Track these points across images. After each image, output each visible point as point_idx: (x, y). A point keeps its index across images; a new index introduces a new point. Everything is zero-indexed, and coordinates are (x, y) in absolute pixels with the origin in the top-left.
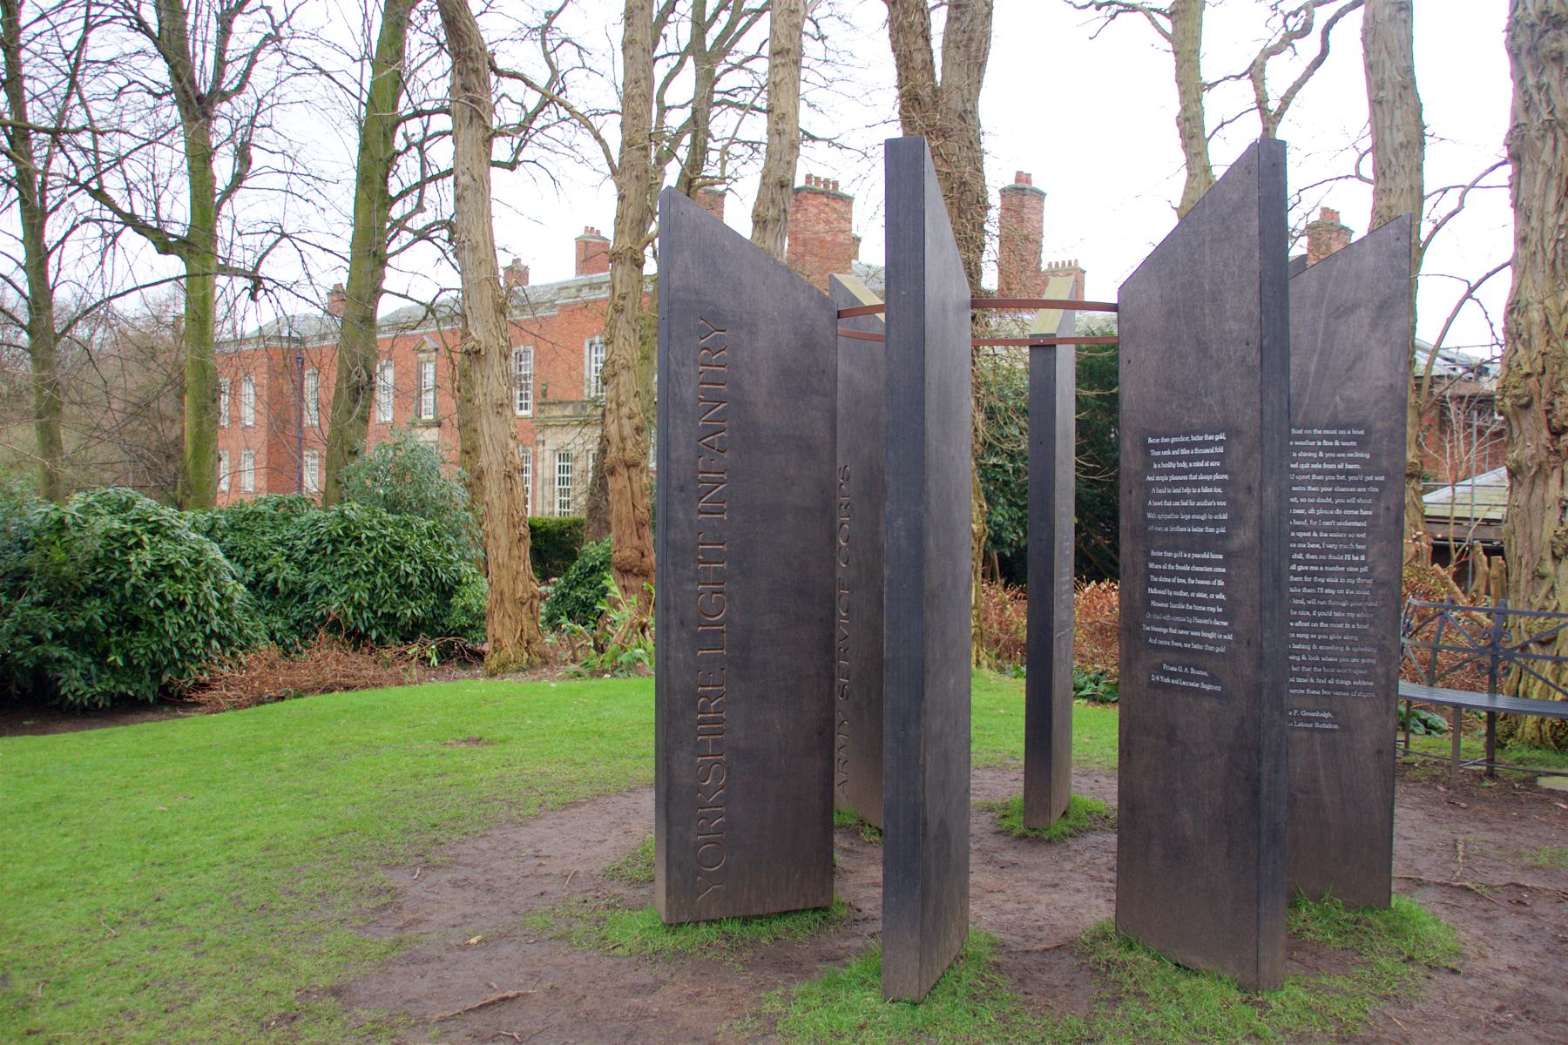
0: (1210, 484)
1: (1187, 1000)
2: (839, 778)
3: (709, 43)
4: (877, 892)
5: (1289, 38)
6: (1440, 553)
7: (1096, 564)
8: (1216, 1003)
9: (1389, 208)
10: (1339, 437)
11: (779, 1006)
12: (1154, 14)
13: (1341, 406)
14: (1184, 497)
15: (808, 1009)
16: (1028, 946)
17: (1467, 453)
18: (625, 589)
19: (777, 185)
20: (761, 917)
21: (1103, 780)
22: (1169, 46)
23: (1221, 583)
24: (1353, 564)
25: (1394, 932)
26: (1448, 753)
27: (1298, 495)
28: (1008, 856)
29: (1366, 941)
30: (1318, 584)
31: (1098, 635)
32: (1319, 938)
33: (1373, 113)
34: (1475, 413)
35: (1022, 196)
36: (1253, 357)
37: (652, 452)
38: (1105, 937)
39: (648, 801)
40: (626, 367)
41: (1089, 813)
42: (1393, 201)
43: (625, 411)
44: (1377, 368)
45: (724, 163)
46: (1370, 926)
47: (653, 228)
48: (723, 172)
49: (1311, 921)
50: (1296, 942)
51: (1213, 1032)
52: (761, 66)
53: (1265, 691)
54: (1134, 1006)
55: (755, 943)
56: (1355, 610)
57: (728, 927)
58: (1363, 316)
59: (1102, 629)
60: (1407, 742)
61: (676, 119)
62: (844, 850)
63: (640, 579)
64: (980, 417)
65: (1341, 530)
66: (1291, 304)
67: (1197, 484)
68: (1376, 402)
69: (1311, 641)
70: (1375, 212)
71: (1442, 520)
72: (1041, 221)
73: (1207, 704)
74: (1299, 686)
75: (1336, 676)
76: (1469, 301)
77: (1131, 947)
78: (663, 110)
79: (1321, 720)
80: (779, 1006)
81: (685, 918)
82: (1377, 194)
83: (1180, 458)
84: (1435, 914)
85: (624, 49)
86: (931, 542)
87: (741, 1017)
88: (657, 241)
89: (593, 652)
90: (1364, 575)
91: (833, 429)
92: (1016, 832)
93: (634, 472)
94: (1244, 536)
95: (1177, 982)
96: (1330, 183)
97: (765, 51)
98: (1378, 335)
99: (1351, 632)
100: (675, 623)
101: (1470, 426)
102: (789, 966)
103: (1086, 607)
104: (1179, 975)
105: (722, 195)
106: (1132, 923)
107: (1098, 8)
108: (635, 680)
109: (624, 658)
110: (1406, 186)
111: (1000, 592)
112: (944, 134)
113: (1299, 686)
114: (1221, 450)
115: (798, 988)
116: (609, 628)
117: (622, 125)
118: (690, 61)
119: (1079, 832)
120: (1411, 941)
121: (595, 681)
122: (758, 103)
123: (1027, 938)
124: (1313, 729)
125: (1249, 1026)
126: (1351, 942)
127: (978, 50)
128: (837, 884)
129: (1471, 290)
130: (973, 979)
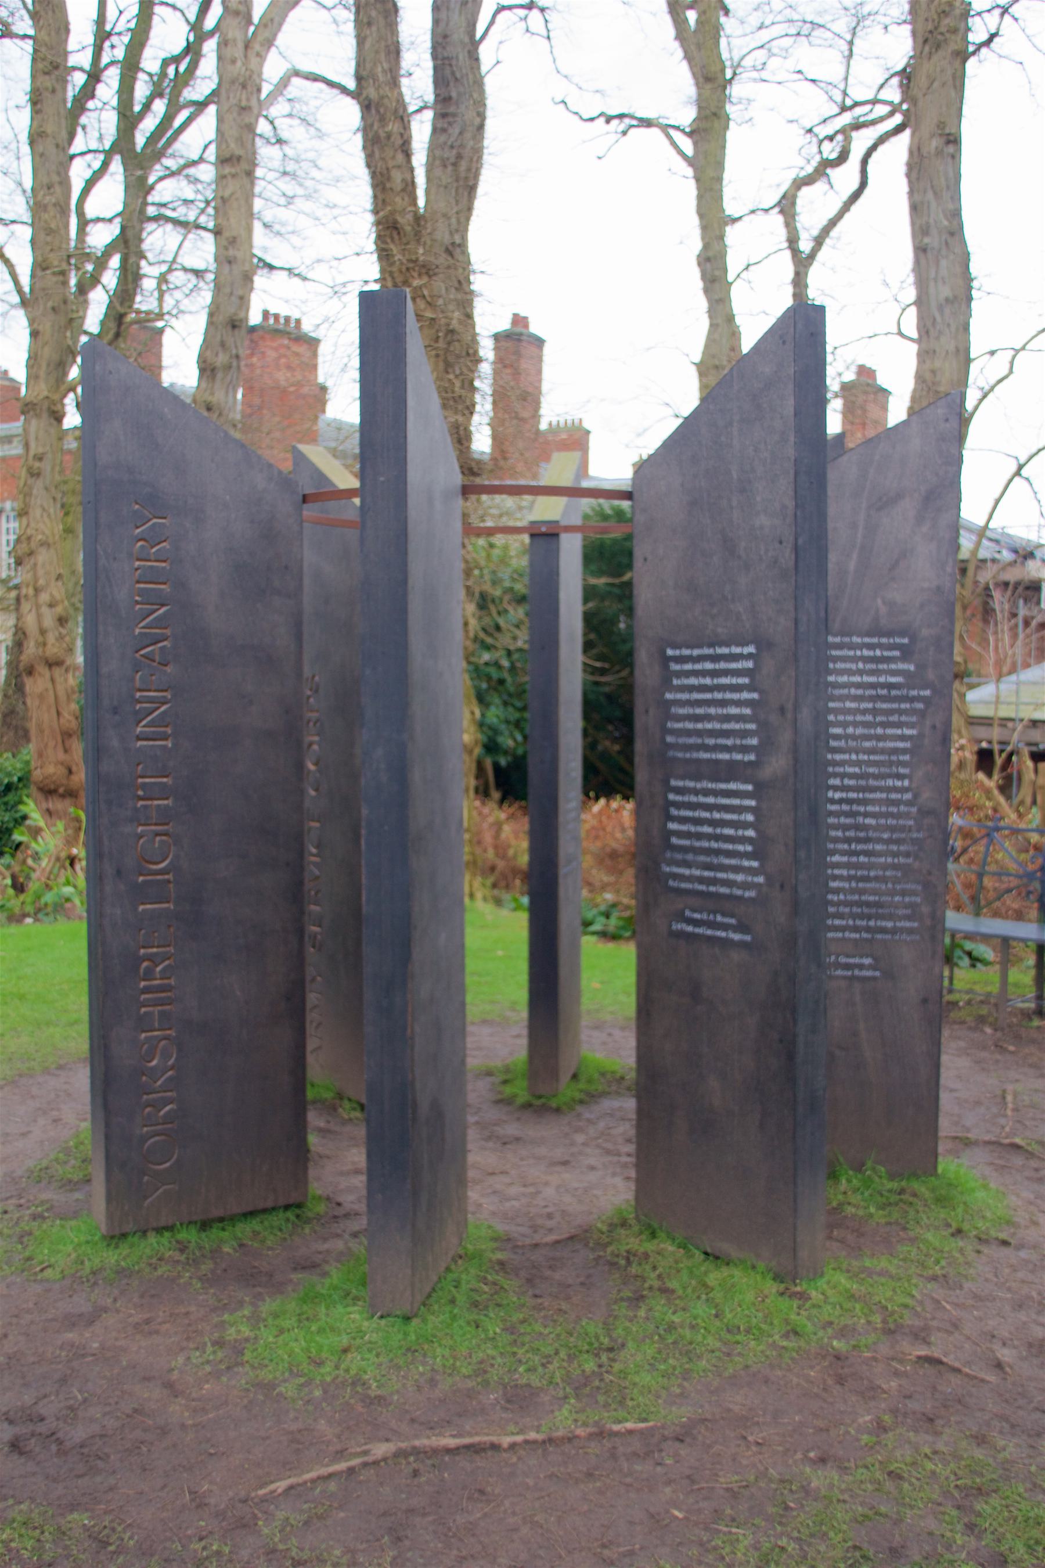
0: (738, 703)
1: (718, 1295)
2: (311, 1044)
3: (140, 140)
4: (360, 1181)
5: (825, 165)
6: (985, 759)
7: (607, 777)
8: (750, 1296)
9: (933, 372)
10: (880, 646)
11: (246, 1331)
12: (672, 132)
13: (883, 610)
14: (707, 718)
15: (281, 1331)
16: (537, 1238)
17: (1012, 646)
18: (49, 813)
19: (227, 325)
20: (221, 1220)
21: (618, 1034)
22: (690, 172)
23: (750, 818)
24: (895, 790)
25: (942, 1201)
26: (995, 989)
27: (836, 711)
28: (511, 1129)
29: (912, 1213)
30: (856, 814)
31: (608, 862)
32: (861, 1213)
33: (917, 261)
34: (1021, 602)
35: (519, 344)
36: (787, 557)
37: (79, 643)
38: (624, 1224)
39: (82, 1080)
40: (45, 544)
41: (603, 1074)
42: (937, 364)
43: (44, 597)
44: (924, 571)
45: (161, 295)
46: (915, 1195)
47: (74, 373)
48: (161, 306)
49: (853, 1193)
50: (836, 1219)
51: (748, 1331)
52: (206, 173)
53: (800, 941)
54: (658, 1304)
55: (216, 1252)
56: (898, 842)
57: (183, 1235)
58: (908, 507)
59: (614, 855)
60: (951, 979)
61: (100, 237)
62: (321, 1130)
63: (68, 801)
64: (471, 608)
65: (883, 751)
66: (829, 493)
67: (723, 703)
68: (922, 606)
69: (849, 878)
70: (919, 377)
71: (986, 722)
72: (539, 372)
73: (736, 956)
74: (836, 929)
75: (878, 917)
76: (1017, 479)
77: (653, 1235)
78: (84, 223)
79: (861, 967)
80: (246, 1331)
81: (129, 1227)
82: (923, 356)
83: (703, 673)
84: (984, 1178)
85: (32, 143)
86: (416, 776)
87: (201, 1348)
88: (79, 390)
89: (11, 892)
90: (909, 803)
91: (299, 637)
92: (520, 1100)
93: (57, 672)
94: (777, 764)
95: (706, 1273)
96: (872, 340)
97: (211, 154)
98: (925, 529)
99: (894, 867)
100: (112, 876)
101: (1014, 615)
102: (255, 1278)
103: (598, 827)
104: (708, 1265)
105: (161, 332)
106: (653, 1209)
107: (608, 121)
108: (63, 926)
109: (49, 898)
110: (951, 347)
111: (494, 813)
112: (427, 270)
113: (836, 929)
114: (750, 664)
115: (268, 1306)
116: (30, 861)
117: (33, 242)
118: (117, 166)
119: (591, 1098)
120: (960, 1210)
121: (14, 929)
122: (203, 220)
123: (535, 1228)
124: (853, 978)
125: (787, 1321)
126: (896, 1215)
127: (469, 170)
128: (312, 1173)
129: (1020, 467)
130: (474, 1284)
